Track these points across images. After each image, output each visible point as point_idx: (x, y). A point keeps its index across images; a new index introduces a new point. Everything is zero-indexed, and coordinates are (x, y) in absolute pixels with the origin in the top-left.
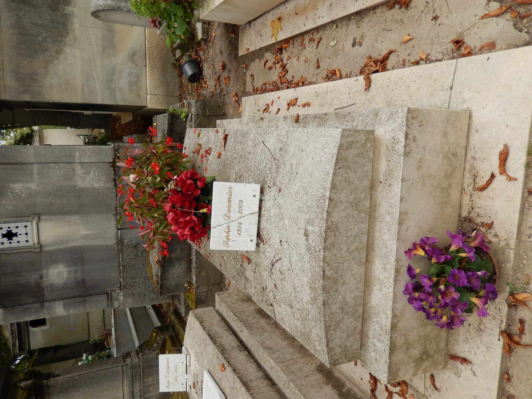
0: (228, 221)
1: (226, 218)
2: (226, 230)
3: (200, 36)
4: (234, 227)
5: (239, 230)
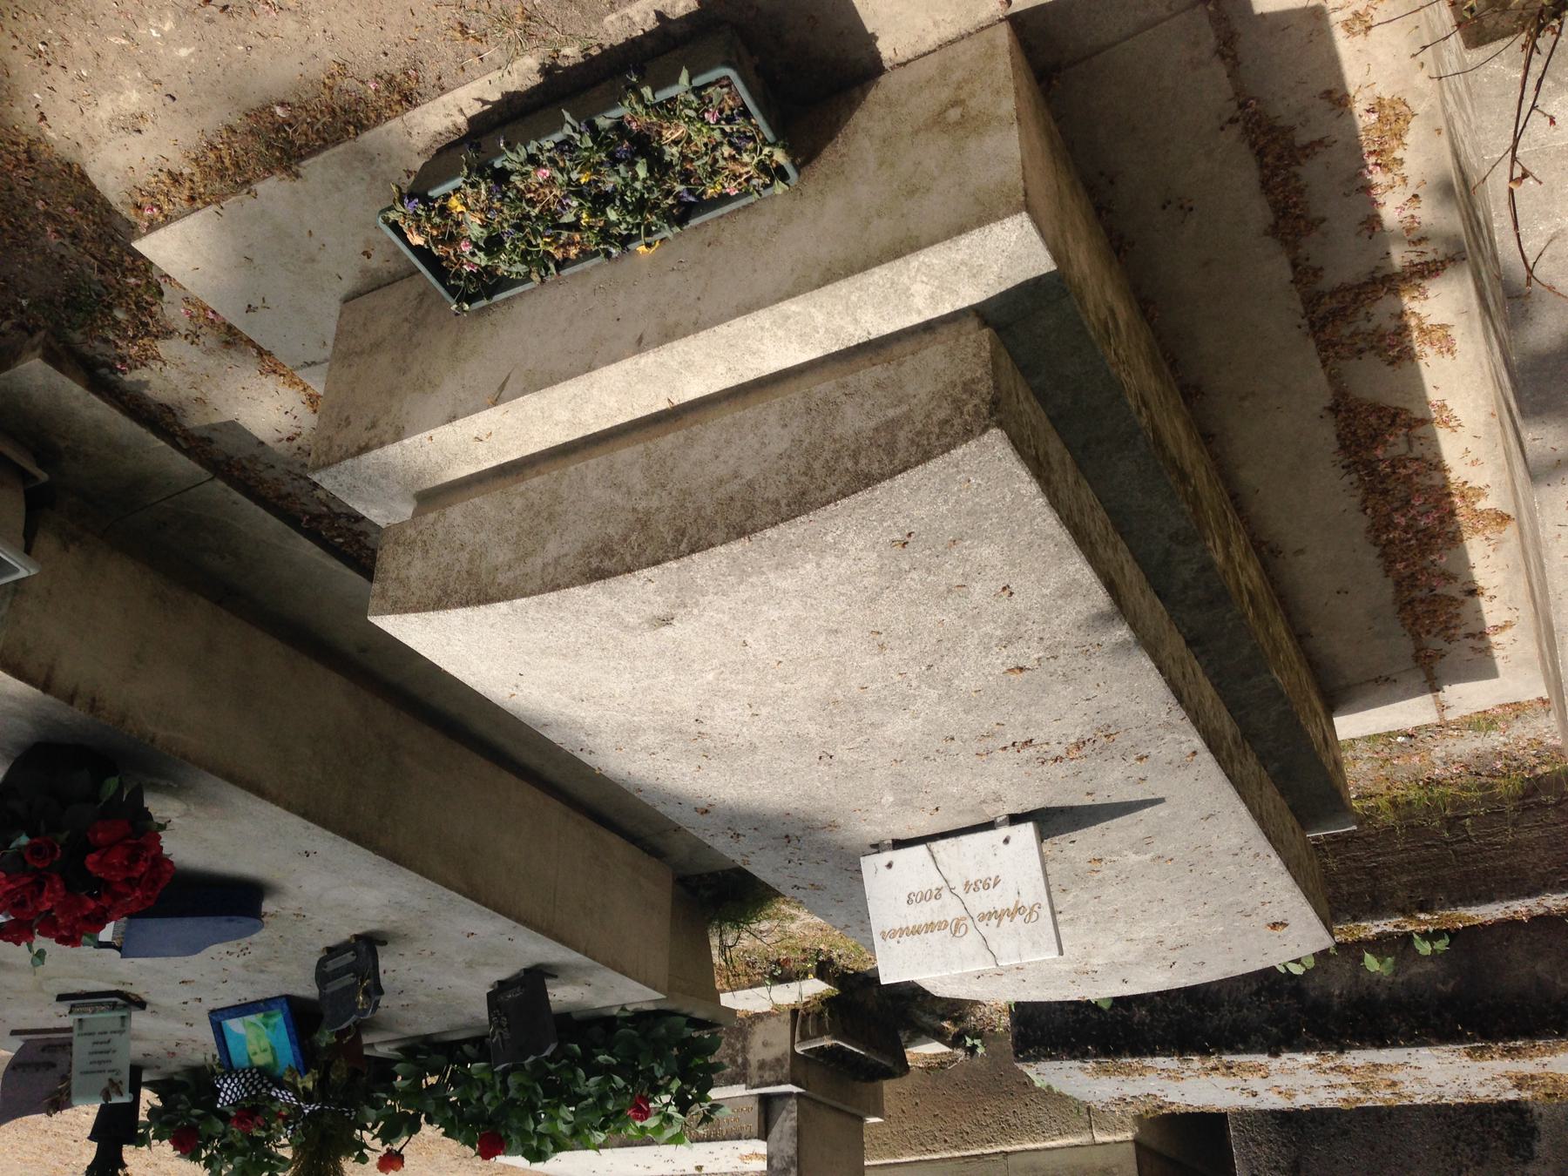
0: (969, 922)
1: (963, 929)
2: (994, 921)
3: (814, 987)
4: (981, 902)
5: (986, 887)
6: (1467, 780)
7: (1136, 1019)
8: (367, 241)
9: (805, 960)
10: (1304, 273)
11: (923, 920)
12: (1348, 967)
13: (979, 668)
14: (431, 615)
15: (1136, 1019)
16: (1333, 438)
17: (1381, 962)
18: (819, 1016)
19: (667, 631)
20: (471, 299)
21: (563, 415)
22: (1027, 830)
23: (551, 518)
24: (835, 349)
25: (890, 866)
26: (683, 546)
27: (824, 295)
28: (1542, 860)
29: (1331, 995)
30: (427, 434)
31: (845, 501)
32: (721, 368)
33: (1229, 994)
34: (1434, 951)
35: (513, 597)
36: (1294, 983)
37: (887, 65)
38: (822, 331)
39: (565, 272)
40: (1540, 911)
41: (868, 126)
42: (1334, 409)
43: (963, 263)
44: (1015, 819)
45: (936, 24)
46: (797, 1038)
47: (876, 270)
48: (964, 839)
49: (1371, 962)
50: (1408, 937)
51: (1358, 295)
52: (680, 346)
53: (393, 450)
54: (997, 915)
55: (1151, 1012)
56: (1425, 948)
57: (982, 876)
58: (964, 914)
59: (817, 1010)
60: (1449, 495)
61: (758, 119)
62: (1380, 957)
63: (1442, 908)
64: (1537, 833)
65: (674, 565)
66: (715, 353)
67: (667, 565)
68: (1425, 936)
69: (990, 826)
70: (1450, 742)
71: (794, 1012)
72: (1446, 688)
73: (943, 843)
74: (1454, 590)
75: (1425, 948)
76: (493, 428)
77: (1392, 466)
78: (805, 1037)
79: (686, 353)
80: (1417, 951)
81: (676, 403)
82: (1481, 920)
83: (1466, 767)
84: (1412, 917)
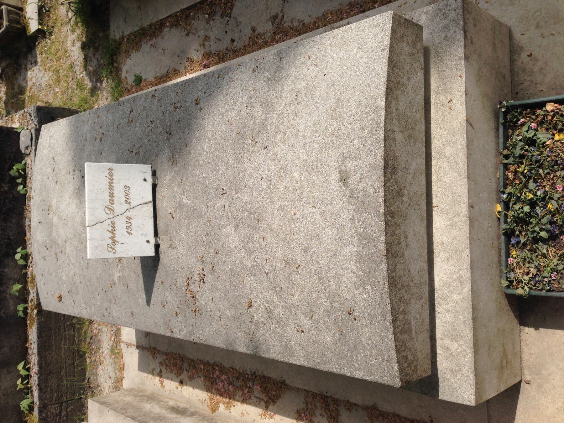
0: (111, 216)
3: (33, 26)
4: (121, 224)
5: (128, 228)
6: (89, 335)
7: (3, 185)
8: (537, 60)
9: (48, 26)
10: (351, 406)
11: (115, 192)
12: (16, 276)
13: (259, 292)
14: (386, 55)
15: (3, 185)
16: (270, 375)
17: (17, 291)
18: (18, 22)
19: (335, 176)
20: (505, 113)
21: (448, 151)
22: (152, 253)
23: (410, 136)
24: (436, 294)
25: (145, 180)
26: (388, 217)
27: (468, 305)
28: (52, 357)
29: (4, 268)
30: (463, 76)
31: (389, 308)
32: (445, 239)
33: (10, 227)
34: (19, 311)
35: (386, 111)
36: (11, 254)
37: (522, 327)
38: (448, 294)
39: (501, 167)
40: (30, 351)
41: (509, 318)
42: (283, 383)
43: (460, 370)
44: (157, 247)
45: (530, 354)
46: (9, 8)
47: (472, 334)
48: (152, 221)
49: (17, 287)
50: (26, 302)
51: (334, 419)
52: (466, 228)
53: (461, 52)
54: (113, 231)
55: (6, 192)
56: (20, 308)
57: (133, 227)
58: (116, 214)
59: (21, 22)
60: (230, 399)
61: (543, 293)
62: (19, 291)
63: (38, 319)
64: (63, 356)
65: (382, 211)
66: (455, 242)
67: (383, 207)
68: (26, 309)
69: (156, 234)
70: (109, 335)
71: (21, 9)
72: (138, 351)
73: (152, 210)
74: (184, 376)
75: (20, 308)
76: (455, 113)
77: (249, 387)
78: (9, 12)
79: (460, 229)
80: (19, 304)
81: (434, 209)
82: (30, 330)
83: (96, 335)
84: (36, 308)
